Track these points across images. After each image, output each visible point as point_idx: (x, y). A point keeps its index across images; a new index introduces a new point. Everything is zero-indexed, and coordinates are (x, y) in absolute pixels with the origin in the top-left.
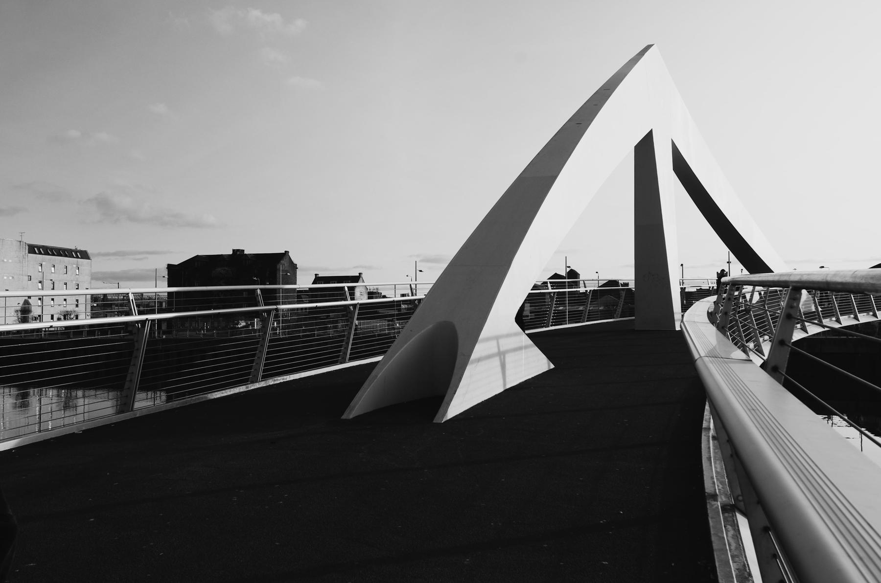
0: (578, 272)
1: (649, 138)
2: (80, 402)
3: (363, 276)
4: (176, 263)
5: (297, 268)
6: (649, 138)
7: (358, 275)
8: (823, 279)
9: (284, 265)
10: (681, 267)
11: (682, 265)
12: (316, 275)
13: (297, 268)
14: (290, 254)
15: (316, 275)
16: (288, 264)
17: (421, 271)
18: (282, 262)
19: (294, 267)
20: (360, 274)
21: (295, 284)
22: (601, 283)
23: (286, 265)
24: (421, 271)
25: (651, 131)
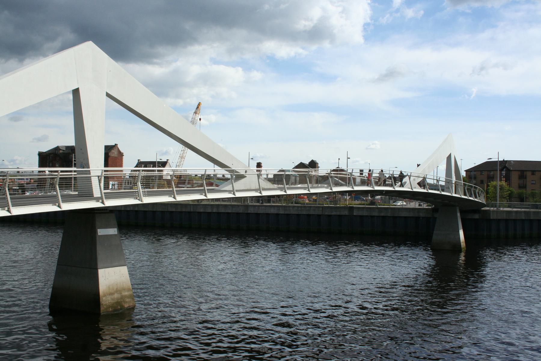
0: (317, 161)
1: (450, 155)
2: (208, 263)
3: (170, 162)
4: (44, 151)
5: (123, 155)
6: (450, 155)
7: (166, 161)
8: (348, 254)
9: (114, 153)
10: (307, 162)
11: (339, 159)
12: (138, 160)
13: (123, 155)
14: (118, 146)
15: (138, 160)
16: (117, 153)
17: (252, 159)
18: (112, 151)
19: (121, 154)
20: (167, 160)
21: (89, 168)
22: (225, 183)
23: (115, 153)
24: (252, 159)
25: (107, 92)
